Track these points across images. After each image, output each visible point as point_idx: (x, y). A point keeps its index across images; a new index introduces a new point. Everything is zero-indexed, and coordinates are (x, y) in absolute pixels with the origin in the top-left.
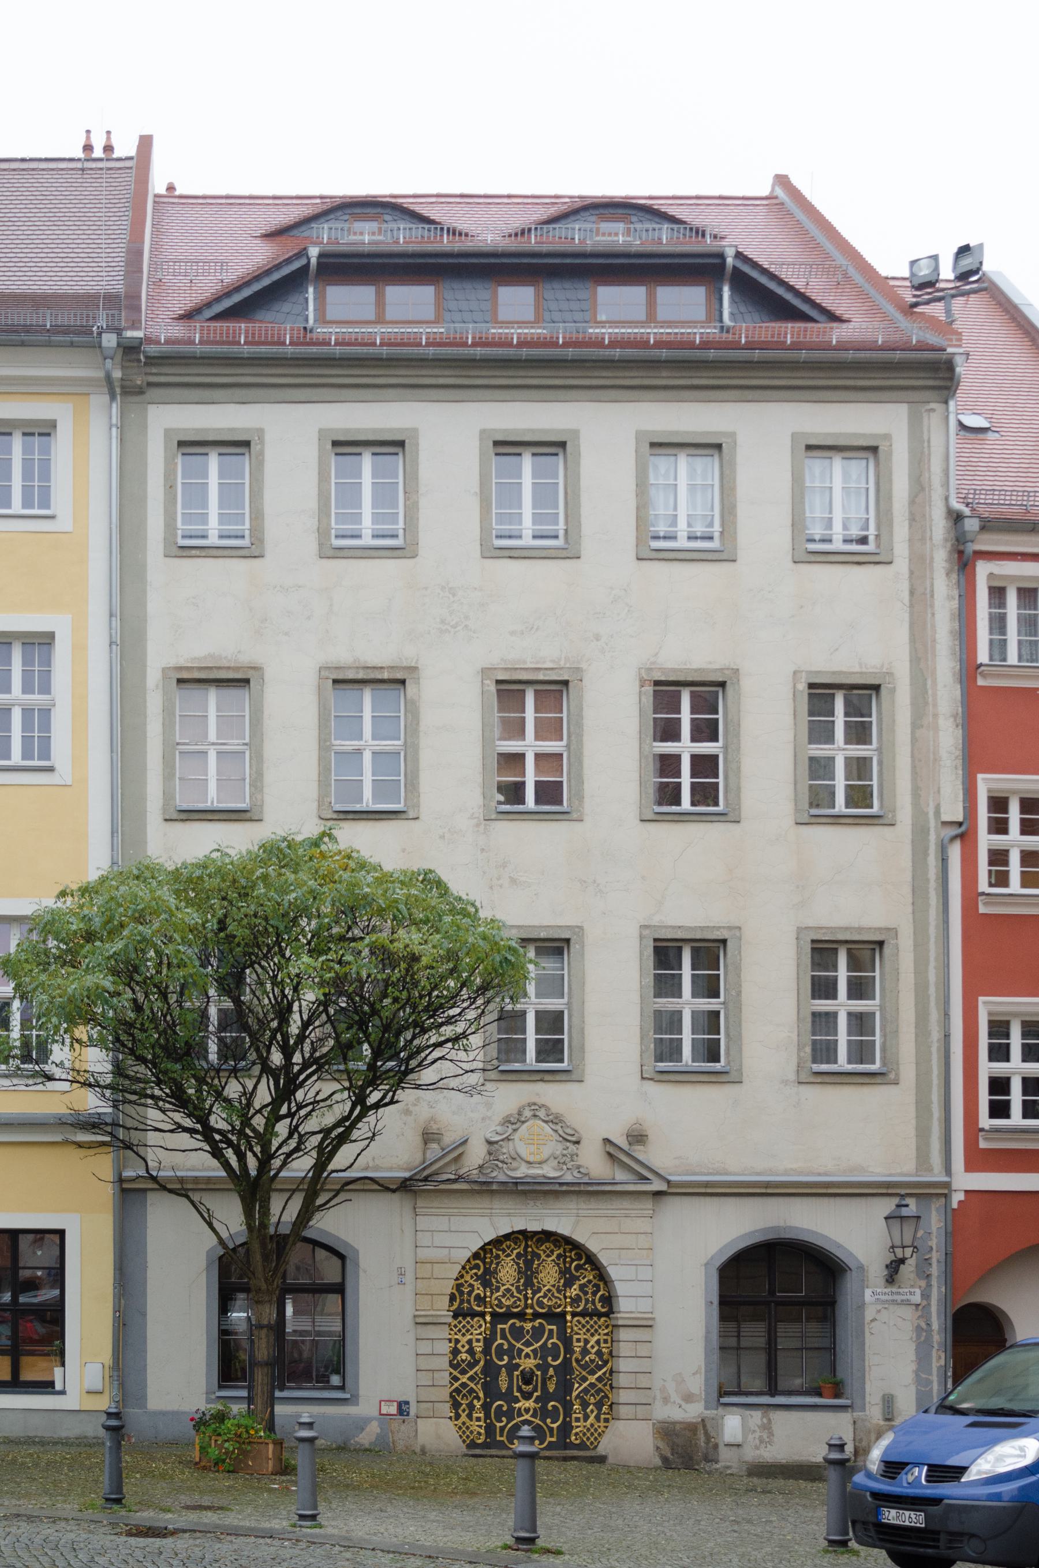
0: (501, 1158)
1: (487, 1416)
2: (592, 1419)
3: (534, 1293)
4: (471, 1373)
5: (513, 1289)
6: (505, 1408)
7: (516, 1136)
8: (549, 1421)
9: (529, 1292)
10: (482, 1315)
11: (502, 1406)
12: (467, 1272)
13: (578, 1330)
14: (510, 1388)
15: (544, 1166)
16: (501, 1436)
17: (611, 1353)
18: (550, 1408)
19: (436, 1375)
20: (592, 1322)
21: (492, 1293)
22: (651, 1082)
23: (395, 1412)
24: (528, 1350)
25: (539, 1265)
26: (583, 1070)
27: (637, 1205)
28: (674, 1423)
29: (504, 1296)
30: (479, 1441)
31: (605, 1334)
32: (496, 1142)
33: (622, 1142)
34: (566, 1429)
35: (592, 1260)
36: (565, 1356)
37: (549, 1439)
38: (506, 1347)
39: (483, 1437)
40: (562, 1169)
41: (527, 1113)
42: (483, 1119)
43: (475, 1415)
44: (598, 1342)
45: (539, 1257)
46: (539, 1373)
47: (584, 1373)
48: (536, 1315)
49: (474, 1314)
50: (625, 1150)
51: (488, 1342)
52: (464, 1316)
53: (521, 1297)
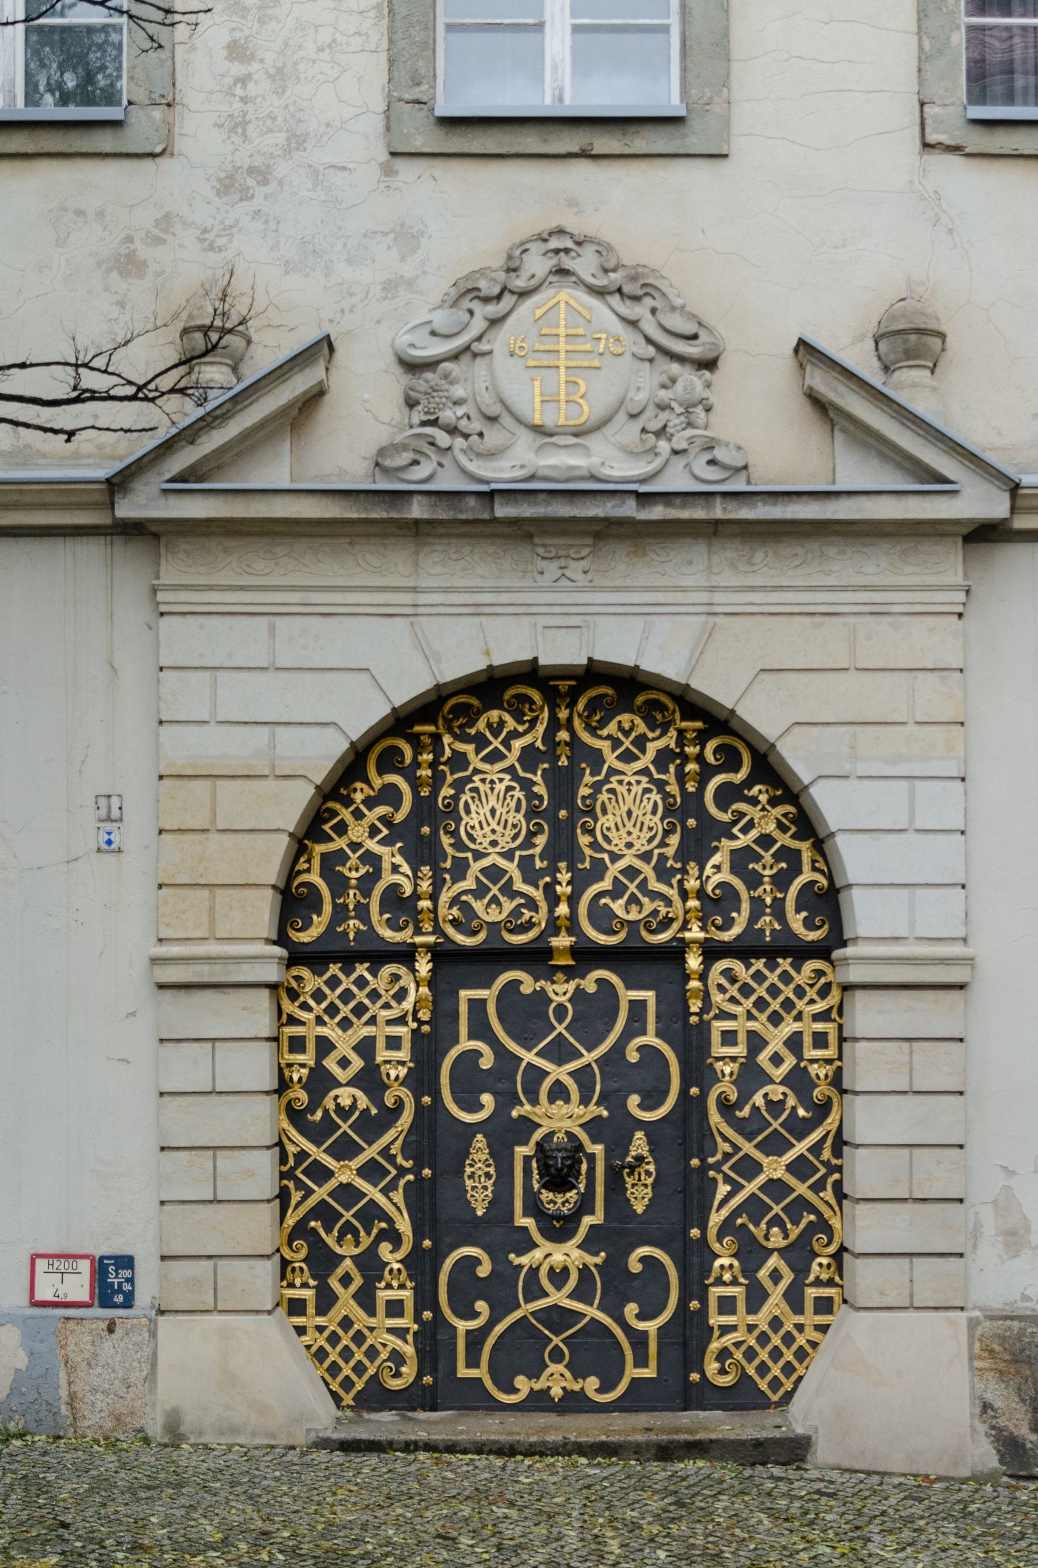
0: (448, 415)
1: (426, 1298)
2: (775, 1303)
3: (579, 883)
4: (371, 1152)
5: (512, 868)
6: (484, 1271)
7: (500, 341)
8: (631, 1309)
9: (564, 876)
10: (406, 956)
11: (477, 1261)
12: (358, 815)
13: (732, 1006)
14: (501, 1202)
15: (593, 442)
16: (473, 1362)
17: (836, 1080)
18: (635, 1267)
19: (225, 1161)
20: (773, 978)
21: (438, 885)
22: (955, 160)
23: (84, 1296)
24: (560, 1073)
25: (597, 787)
26: (727, 123)
27: (911, 573)
29: (480, 892)
30: (395, 1384)
31: (817, 1017)
32: (431, 365)
33: (861, 359)
34: (688, 1337)
36: (684, 1092)
37: (632, 1372)
39: (409, 1371)
40: (653, 452)
41: (537, 264)
42: (390, 287)
43: (383, 1295)
44: (794, 1043)
45: (596, 759)
46: (598, 1149)
47: (748, 1148)
48: (587, 956)
49: (380, 955)
51: (428, 1049)
52: (349, 959)
53: (538, 894)
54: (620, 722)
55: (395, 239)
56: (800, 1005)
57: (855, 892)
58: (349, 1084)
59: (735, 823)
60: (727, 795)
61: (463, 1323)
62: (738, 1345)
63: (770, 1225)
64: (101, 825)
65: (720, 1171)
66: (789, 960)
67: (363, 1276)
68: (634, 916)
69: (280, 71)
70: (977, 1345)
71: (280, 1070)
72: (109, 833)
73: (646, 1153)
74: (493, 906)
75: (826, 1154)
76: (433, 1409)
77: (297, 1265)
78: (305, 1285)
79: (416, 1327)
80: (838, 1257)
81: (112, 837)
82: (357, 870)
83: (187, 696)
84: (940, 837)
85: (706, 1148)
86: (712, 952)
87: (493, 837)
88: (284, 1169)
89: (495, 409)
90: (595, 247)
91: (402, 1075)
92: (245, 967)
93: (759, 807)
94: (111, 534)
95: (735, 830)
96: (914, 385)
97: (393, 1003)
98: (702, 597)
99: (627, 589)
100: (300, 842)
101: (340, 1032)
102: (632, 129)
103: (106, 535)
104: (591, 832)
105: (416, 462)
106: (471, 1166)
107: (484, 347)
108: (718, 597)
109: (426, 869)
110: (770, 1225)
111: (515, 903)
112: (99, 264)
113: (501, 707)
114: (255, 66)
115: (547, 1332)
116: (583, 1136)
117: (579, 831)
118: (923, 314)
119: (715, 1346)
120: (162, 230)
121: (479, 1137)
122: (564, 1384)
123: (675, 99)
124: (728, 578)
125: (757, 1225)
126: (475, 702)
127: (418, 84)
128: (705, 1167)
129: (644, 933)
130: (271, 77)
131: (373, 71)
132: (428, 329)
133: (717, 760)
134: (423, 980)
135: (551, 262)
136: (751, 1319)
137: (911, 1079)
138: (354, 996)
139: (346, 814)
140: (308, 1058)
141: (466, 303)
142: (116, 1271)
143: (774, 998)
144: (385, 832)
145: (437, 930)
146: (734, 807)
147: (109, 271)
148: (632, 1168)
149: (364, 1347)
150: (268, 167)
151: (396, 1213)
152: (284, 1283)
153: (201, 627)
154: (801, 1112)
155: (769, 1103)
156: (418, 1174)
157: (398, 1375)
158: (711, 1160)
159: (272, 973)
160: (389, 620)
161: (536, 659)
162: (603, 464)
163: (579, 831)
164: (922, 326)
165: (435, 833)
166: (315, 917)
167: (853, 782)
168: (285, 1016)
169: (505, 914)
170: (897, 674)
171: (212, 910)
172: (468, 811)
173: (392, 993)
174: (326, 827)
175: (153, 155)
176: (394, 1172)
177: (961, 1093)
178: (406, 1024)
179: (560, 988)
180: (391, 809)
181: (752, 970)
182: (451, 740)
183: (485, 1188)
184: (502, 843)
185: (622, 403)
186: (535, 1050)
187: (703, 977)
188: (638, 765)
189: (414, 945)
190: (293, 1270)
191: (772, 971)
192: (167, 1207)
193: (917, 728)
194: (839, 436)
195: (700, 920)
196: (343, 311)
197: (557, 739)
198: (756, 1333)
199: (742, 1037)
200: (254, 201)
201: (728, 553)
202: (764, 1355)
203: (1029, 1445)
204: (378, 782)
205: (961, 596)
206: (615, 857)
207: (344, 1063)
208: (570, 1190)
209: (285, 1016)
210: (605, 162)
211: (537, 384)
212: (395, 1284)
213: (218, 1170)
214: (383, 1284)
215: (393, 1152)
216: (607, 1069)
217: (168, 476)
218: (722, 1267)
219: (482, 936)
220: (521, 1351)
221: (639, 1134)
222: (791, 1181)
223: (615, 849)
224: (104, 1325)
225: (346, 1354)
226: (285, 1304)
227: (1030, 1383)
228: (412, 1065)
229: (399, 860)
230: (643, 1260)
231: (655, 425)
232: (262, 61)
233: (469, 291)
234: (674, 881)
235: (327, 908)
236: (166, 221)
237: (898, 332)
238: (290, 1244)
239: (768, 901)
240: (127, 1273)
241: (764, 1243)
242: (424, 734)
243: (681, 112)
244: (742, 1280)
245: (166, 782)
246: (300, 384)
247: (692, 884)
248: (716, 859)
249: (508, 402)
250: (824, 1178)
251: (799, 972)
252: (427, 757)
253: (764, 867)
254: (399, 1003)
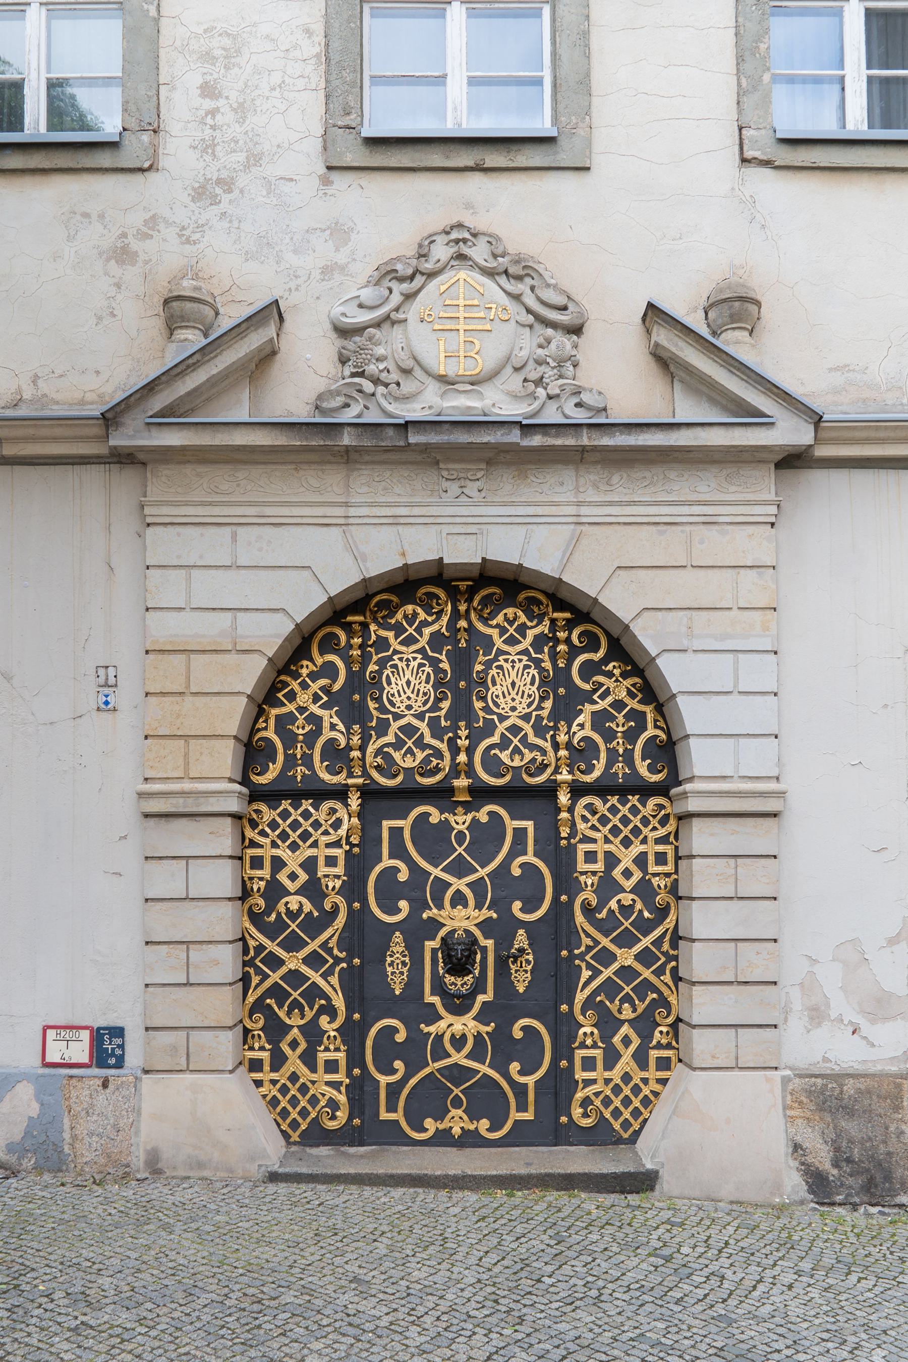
0: (372, 368)
1: (355, 1058)
2: (626, 1063)
4: (313, 945)
5: (423, 727)
6: (400, 1037)
8: (515, 1067)
9: (463, 733)
10: (341, 794)
11: (396, 1030)
13: (589, 827)
14: (414, 984)
16: (391, 1108)
17: (673, 889)
18: (518, 1034)
19: (196, 954)
20: (624, 810)
21: (365, 740)
23: (85, 1059)
24: (460, 884)
25: (488, 665)
28: (839, 1078)
29: (398, 745)
30: (332, 1125)
31: (658, 841)
32: (359, 330)
34: (558, 1088)
35: (623, 651)
37: (515, 1115)
38: (403, 876)
40: (533, 396)
41: (441, 252)
42: (327, 271)
43: (322, 1056)
44: (641, 861)
45: (488, 642)
46: (489, 943)
47: (605, 942)
48: (481, 794)
50: (706, 339)
51: (358, 865)
52: (297, 796)
53: (443, 747)
54: (506, 614)
55: (331, 234)
56: (645, 831)
57: (692, 741)
58: (296, 893)
59: (595, 691)
60: (588, 670)
61: (384, 1077)
62: (597, 1095)
63: (622, 1001)
64: (100, 689)
65: (583, 960)
66: (637, 797)
67: (307, 1041)
68: (517, 763)
69: (241, 105)
70: (789, 1097)
71: (243, 881)
72: (107, 696)
73: (526, 947)
74: (409, 756)
75: (666, 946)
76: (361, 1144)
77: (256, 1033)
78: (262, 1048)
79: (348, 1080)
80: (674, 1026)
81: (109, 699)
82: (303, 728)
83: (168, 589)
84: (758, 698)
85: (573, 942)
86: (578, 790)
87: (408, 703)
88: (247, 959)
89: (409, 363)
90: (487, 239)
91: (338, 885)
92: (212, 800)
93: (614, 679)
94: (109, 463)
95: (595, 697)
96: (738, 342)
97: (331, 831)
98: (572, 510)
99: (512, 504)
100: (260, 706)
101: (290, 853)
102: (515, 147)
103: (105, 463)
104: (484, 699)
105: (347, 405)
106: (391, 956)
107: (401, 316)
108: (584, 510)
109: (356, 727)
110: (622, 1001)
111: (426, 753)
112: (100, 254)
113: (414, 602)
114: (221, 102)
115: (449, 1084)
116: (477, 933)
117: (474, 698)
118: (744, 286)
119: (579, 1095)
120: (149, 228)
121: (397, 934)
122: (462, 1125)
123: (548, 123)
124: (592, 495)
125: (612, 1002)
126: (395, 599)
127: (348, 114)
128: (572, 957)
129: (525, 776)
130: (233, 110)
131: (315, 104)
132: (357, 302)
133: (581, 642)
134: (353, 812)
135: (452, 250)
136: (607, 1074)
137: (736, 887)
138: (301, 825)
139: (295, 685)
140: (266, 873)
141: (386, 283)
142: (110, 1039)
143: (625, 827)
144: (325, 699)
145: (365, 774)
146: (594, 679)
147: (108, 260)
148: (516, 958)
149: (308, 1097)
150: (232, 178)
151: (333, 993)
152: (246, 1047)
153: (179, 534)
154: (646, 914)
155: (622, 907)
156: (350, 963)
157: (333, 1118)
158: (576, 952)
159: (234, 805)
160: (325, 529)
161: (441, 559)
162: (494, 405)
163: (474, 698)
164: (744, 295)
165: (363, 699)
166: (271, 764)
167: (690, 656)
168: (247, 841)
169: (417, 762)
170: (724, 570)
171: (186, 755)
172: (389, 683)
173: (330, 822)
174: (280, 695)
175: (141, 170)
176: (331, 961)
177: (775, 899)
178: (341, 847)
179: (460, 819)
180: (329, 681)
181: (609, 805)
182: (376, 628)
183: (402, 973)
184: (416, 708)
185: (509, 359)
186: (441, 867)
187: (571, 810)
188: (520, 647)
189: (347, 785)
190: (253, 1036)
191: (624, 805)
192: (150, 989)
193: (740, 612)
194: (677, 386)
195: (568, 766)
196: (290, 289)
197: (458, 626)
198: (611, 1085)
199: (600, 856)
200: (221, 205)
201: (592, 476)
202: (617, 1102)
203: (831, 1178)
204: (319, 661)
205: (773, 510)
206: (502, 718)
207: (293, 877)
208: (467, 975)
209: (247, 841)
210: (494, 175)
211: (442, 343)
212: (332, 1047)
213: (190, 960)
214: (322, 1048)
215: (330, 945)
216: (496, 881)
217: (151, 413)
218: (585, 1034)
219: (400, 778)
220: (429, 1100)
221: (521, 932)
222: (639, 967)
223: (502, 712)
224: (99, 1082)
225: (294, 1102)
226: (247, 1063)
227: (831, 1127)
228: (345, 878)
229: (335, 720)
230: (523, 1028)
231: (534, 376)
232: (227, 98)
233: (388, 272)
234: (548, 737)
235: (280, 758)
236: (153, 222)
237: (725, 300)
238: (250, 1017)
239: (621, 751)
240: (119, 1041)
241: (618, 1015)
242: (355, 623)
243: (554, 133)
244: (600, 1044)
245: (151, 656)
246: (255, 340)
247: (562, 738)
248: (580, 719)
249: (419, 358)
250: (664, 965)
251: (644, 806)
252: (357, 641)
253: (618, 726)
254: (336, 831)
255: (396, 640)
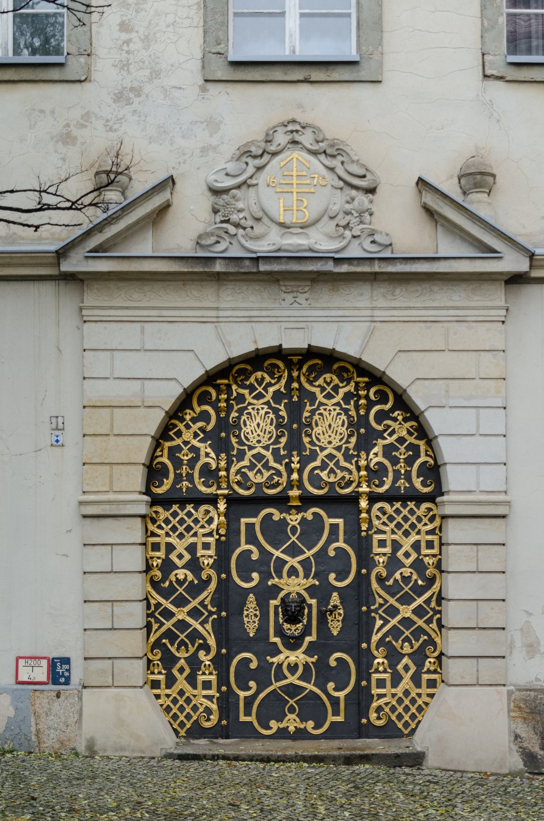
0: (235, 217)
1: (223, 679)
2: (406, 682)
3: (304, 462)
4: (194, 603)
5: (268, 455)
6: (254, 665)
7: (262, 178)
8: (331, 686)
9: (296, 459)
10: (213, 500)
11: (250, 660)
12: (188, 427)
13: (383, 527)
14: (263, 629)
15: (311, 231)
16: (248, 713)
17: (438, 566)
18: (333, 663)
19: (118, 608)
20: (405, 512)
21: (229, 463)
22: (500, 84)
23: (44, 679)
24: (293, 562)
25: (313, 412)
26: (381, 64)
27: (477, 300)
29: (251, 467)
30: (207, 725)
31: (428, 533)
32: (226, 191)
33: (451, 188)
34: (360, 700)
36: (358, 572)
37: (331, 718)
39: (214, 718)
40: (342, 237)
41: (281, 138)
42: (204, 150)
43: (201, 678)
44: (416, 546)
45: (312, 397)
46: (314, 602)
47: (392, 601)
48: (308, 501)
49: (199, 500)
51: (224, 549)
52: (183, 502)
53: (282, 468)
54: (325, 378)
55: (207, 125)
56: (419, 526)
57: (448, 467)
58: (183, 568)
59: (385, 431)
60: (381, 416)
61: (242, 693)
62: (387, 704)
63: (403, 641)
64: (53, 432)
65: (377, 613)
66: (414, 503)
67: (190, 668)
68: (332, 479)
69: (147, 37)
70: (512, 704)
71: (147, 560)
72: (57, 436)
73: (338, 604)
74: (259, 474)
75: (433, 604)
76: (227, 738)
77: (156, 662)
78: (160, 673)
79: (218, 695)
80: (439, 658)
81: (59, 438)
82: (187, 455)
83: (98, 364)
84: (492, 438)
85: (370, 601)
86: (373, 499)
87: (258, 438)
88: (149, 612)
89: (259, 214)
90: (312, 130)
91: (211, 563)
92: (129, 506)
93: (398, 423)
94: (58, 280)
95: (385, 435)
96: (479, 202)
97: (206, 525)
98: (368, 313)
99: (328, 308)
100: (157, 441)
101: (178, 540)
102: (331, 67)
103: (55, 280)
104: (310, 436)
105: (218, 242)
106: (247, 610)
107: (254, 181)
108: (377, 313)
109: (223, 455)
110: (403, 641)
111: (270, 473)
112: (52, 138)
113: (262, 370)
114: (134, 35)
115: (286, 698)
116: (306, 595)
117: (303, 435)
118: (484, 164)
119: (375, 705)
120: (85, 121)
121: (251, 595)
122: (295, 725)
123: (354, 52)
124: (381, 302)
125: (397, 641)
126: (249, 367)
127: (219, 44)
128: (369, 611)
129: (337, 489)
130: (142, 40)
131: (196, 37)
132: (224, 172)
133: (376, 398)
134: (222, 513)
135: (289, 137)
136: (393, 691)
137: (477, 565)
138: (186, 522)
139: (181, 426)
140: (162, 554)
141: (244, 159)
142: (61, 666)
143: (406, 523)
144: (202, 435)
145: (229, 487)
146: (385, 422)
147: (57, 142)
148: (331, 612)
149: (191, 706)
150: (141, 87)
151: (208, 635)
152: (149, 672)
153: (105, 328)
154: (420, 582)
155: (403, 577)
156: (219, 615)
157: (208, 720)
158: (373, 608)
159: (143, 510)
160: (204, 325)
161: (281, 345)
162: (316, 243)
163: (303, 435)
164: (483, 171)
165: (228, 436)
166: (165, 480)
167: (447, 410)
168: (149, 532)
169: (264, 479)
170: (470, 353)
171: (111, 476)
172: (245, 425)
173: (205, 520)
174: (171, 433)
175: (80, 81)
176: (206, 614)
177: (504, 572)
178: (213, 536)
179: (293, 517)
180: (205, 424)
181: (394, 508)
182: (237, 387)
183: (254, 622)
184: (263, 442)
185: (326, 211)
186: (281, 550)
187: (368, 512)
188: (334, 401)
189: (217, 495)
190: (154, 665)
191: (405, 508)
192: (88, 632)
193: (481, 381)
194: (439, 228)
195: (367, 482)
196: (180, 163)
197: (292, 387)
198: (396, 698)
199: (389, 543)
200: (133, 105)
201: (381, 289)
202: (400, 709)
203: (539, 757)
204: (198, 409)
205: (504, 312)
206: (322, 449)
207: (180, 556)
208: (299, 623)
209: (149, 532)
210: (317, 85)
211: (281, 201)
212: (207, 672)
213: (114, 613)
214: (201, 672)
215: (206, 603)
216: (318, 560)
217: (88, 249)
218: (378, 663)
219: (253, 490)
220: (273, 708)
221: (335, 594)
222: (415, 618)
223: (322, 445)
224: (54, 694)
225: (182, 709)
226: (149, 683)
227: (540, 724)
228: (216, 558)
229: (209, 450)
230: (337, 660)
231: (343, 223)
232: (137, 32)
233: (246, 152)
234: (353, 462)
235: (172, 476)
236: (87, 116)
237: (471, 174)
238: (152, 651)
239: (403, 472)
240: (67, 667)
241: (401, 651)
242: (222, 384)
243: (357, 59)
244: (389, 670)
245: (87, 409)
246: (157, 201)
247: (363, 463)
248: (375, 450)
249: (266, 210)
250: (432, 617)
251: (419, 509)
252: (224, 396)
253: (401, 454)
254: (209, 525)
255: (268, 459)
